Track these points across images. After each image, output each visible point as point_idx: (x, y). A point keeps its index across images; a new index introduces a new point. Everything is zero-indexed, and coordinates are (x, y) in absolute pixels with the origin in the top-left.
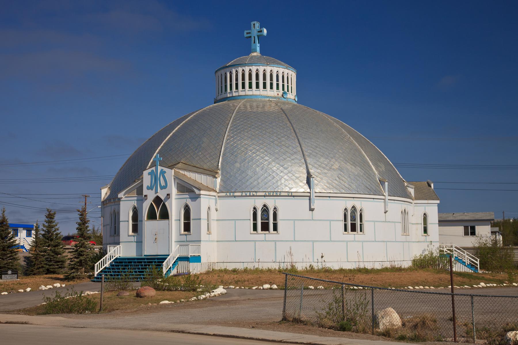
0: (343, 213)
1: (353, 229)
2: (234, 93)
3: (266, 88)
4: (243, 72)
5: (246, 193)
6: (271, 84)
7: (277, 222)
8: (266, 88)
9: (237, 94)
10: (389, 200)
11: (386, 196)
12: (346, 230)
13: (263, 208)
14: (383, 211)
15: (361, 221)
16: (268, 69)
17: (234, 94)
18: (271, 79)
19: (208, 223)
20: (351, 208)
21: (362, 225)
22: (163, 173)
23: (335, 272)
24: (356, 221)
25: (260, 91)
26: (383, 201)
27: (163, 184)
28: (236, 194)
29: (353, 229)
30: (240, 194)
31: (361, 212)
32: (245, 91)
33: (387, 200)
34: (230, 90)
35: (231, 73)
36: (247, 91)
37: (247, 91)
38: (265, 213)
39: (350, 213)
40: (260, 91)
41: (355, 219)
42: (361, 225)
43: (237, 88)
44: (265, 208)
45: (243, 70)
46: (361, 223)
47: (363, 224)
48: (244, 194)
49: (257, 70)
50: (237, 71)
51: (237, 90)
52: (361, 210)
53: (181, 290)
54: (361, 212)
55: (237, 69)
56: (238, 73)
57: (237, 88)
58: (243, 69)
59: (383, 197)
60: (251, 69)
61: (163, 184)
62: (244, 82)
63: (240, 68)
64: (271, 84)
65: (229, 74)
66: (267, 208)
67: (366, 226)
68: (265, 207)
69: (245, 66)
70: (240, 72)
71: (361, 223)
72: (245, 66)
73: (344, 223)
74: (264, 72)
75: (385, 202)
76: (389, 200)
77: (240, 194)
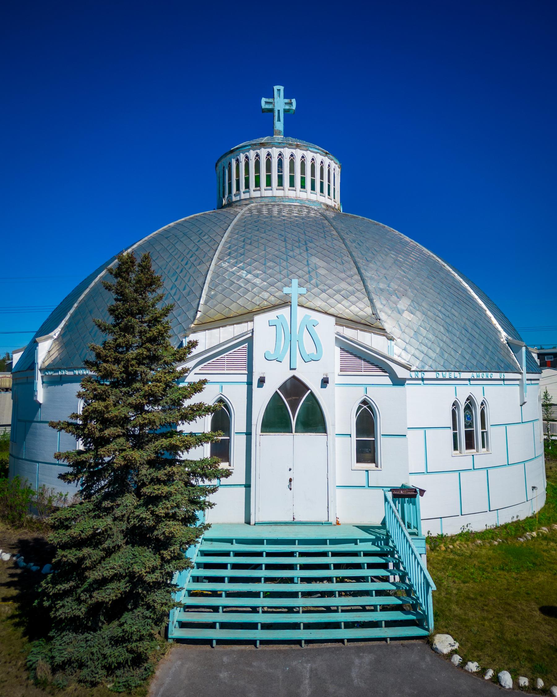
0: (451, 409)
1: (470, 445)
2: (233, 197)
3: (294, 187)
4: (257, 158)
5: (444, 373)
6: (292, 179)
7: (486, 430)
8: (294, 187)
9: (247, 196)
10: (528, 380)
11: (524, 374)
12: (455, 448)
13: (360, 407)
14: (519, 403)
15: (483, 426)
16: (298, 153)
17: (243, 196)
18: (292, 169)
19: (455, 435)
20: (465, 401)
21: (485, 433)
22: (310, 327)
23: (453, 539)
24: (473, 428)
25: (295, 191)
26: (518, 382)
27: (309, 348)
28: (427, 375)
29: (470, 445)
30: (433, 375)
31: (482, 407)
32: (260, 190)
33: (525, 380)
34: (237, 191)
35: (238, 161)
36: (263, 190)
37: (263, 190)
38: (467, 414)
39: (463, 408)
40: (272, 190)
41: (472, 421)
42: (483, 433)
43: (247, 186)
44: (365, 407)
45: (269, 154)
46: (484, 430)
47: (486, 432)
48: (440, 376)
49: (280, 155)
50: (247, 157)
51: (247, 190)
52: (482, 404)
53: (299, 607)
54: (482, 407)
55: (247, 153)
56: (248, 160)
57: (247, 186)
58: (268, 152)
59: (518, 376)
60: (259, 153)
61: (309, 348)
62: (259, 176)
63: (251, 151)
64: (292, 179)
65: (235, 162)
66: (370, 407)
67: (495, 435)
68: (365, 405)
69: (284, 147)
70: (241, 161)
71: (484, 430)
72: (272, 147)
73: (452, 432)
74: (280, 157)
75: (521, 386)
76: (528, 380)
77: (433, 375)
